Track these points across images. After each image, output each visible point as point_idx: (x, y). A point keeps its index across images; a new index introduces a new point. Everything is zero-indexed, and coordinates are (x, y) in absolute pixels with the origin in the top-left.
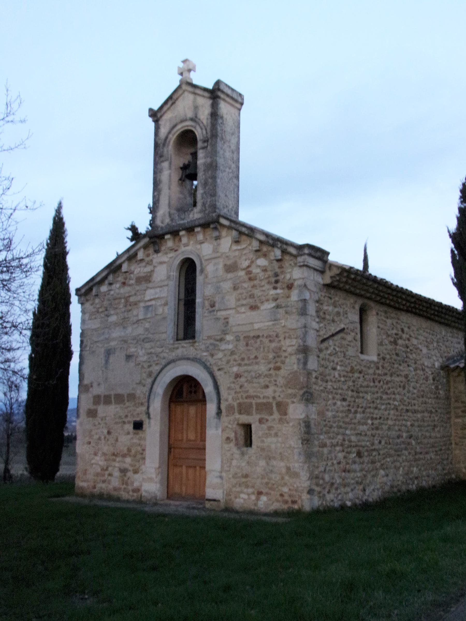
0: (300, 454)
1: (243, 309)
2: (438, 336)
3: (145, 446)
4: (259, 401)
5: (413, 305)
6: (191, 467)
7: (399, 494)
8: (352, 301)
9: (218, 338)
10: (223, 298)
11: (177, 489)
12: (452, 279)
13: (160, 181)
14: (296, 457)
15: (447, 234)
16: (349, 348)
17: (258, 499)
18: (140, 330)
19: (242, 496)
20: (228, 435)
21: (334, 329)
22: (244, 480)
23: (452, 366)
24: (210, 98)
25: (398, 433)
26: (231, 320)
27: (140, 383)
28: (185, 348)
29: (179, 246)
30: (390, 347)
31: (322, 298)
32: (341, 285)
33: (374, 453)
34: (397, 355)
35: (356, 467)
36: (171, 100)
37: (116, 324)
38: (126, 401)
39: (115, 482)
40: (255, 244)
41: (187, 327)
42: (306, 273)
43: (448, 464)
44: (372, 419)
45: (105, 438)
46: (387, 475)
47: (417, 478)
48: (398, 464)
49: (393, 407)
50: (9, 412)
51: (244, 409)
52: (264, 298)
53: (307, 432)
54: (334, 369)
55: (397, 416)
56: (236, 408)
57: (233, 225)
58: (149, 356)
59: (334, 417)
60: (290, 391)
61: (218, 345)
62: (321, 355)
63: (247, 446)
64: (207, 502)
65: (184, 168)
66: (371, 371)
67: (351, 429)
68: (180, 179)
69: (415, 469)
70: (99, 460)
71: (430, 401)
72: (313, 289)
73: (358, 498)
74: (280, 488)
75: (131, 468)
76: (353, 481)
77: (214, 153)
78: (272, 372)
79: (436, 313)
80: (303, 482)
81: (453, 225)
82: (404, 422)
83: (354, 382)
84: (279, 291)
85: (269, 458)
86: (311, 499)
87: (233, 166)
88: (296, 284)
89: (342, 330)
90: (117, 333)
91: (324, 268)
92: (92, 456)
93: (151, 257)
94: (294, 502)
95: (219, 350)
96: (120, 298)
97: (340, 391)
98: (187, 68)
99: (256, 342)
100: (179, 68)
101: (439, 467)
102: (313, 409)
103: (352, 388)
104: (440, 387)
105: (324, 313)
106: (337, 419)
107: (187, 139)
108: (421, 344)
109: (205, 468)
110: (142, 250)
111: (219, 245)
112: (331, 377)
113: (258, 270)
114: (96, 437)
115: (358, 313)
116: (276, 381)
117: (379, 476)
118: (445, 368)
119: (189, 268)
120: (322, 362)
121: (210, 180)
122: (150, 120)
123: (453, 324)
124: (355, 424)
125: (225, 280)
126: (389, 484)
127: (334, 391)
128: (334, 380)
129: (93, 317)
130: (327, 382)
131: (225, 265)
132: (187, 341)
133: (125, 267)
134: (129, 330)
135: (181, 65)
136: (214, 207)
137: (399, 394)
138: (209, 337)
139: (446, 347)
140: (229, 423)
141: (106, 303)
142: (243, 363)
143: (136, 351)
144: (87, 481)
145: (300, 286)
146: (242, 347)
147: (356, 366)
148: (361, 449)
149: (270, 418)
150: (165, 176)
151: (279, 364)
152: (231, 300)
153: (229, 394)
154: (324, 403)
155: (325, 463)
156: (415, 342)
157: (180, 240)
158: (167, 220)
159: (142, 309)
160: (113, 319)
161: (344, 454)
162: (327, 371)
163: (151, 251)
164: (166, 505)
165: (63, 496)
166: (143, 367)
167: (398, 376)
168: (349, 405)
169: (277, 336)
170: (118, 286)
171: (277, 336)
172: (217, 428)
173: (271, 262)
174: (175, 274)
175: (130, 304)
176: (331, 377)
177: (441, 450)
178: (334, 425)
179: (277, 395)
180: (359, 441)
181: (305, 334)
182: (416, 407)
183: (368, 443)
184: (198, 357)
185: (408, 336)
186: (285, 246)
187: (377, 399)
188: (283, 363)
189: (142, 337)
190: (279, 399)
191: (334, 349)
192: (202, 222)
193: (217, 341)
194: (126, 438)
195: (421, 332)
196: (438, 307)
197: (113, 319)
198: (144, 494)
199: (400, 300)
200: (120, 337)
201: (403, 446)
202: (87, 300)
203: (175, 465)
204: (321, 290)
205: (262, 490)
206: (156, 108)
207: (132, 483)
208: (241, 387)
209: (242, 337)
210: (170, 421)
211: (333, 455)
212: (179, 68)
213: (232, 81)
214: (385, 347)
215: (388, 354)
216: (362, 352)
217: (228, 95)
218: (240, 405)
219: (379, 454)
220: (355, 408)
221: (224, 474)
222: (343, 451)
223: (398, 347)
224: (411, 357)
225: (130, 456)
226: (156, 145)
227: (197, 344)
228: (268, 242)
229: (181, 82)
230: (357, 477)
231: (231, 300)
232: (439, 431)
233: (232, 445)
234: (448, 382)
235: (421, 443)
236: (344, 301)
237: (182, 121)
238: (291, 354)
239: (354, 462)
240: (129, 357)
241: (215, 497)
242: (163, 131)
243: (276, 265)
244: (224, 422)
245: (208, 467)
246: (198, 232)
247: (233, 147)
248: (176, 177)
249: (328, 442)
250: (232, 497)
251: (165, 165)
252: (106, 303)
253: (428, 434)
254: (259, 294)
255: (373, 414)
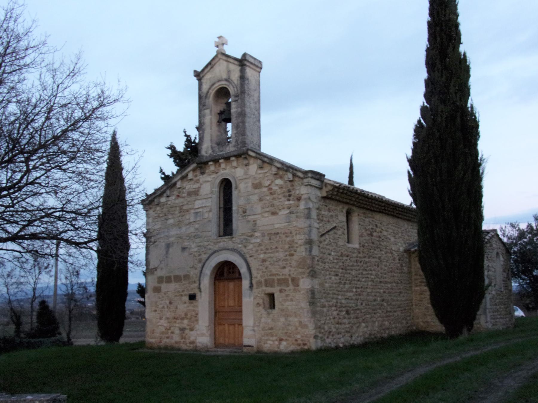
0: (308, 312)
1: (266, 215)
2: (403, 229)
3: (198, 311)
4: (279, 277)
5: (383, 208)
6: (231, 325)
7: (375, 340)
8: (341, 207)
9: (250, 234)
10: (252, 207)
11: (221, 341)
12: (409, 191)
13: (204, 124)
14: (305, 315)
15: (406, 160)
16: (340, 239)
17: (280, 344)
18: (192, 230)
19: (269, 342)
20: (258, 302)
21: (329, 227)
22: (270, 331)
23: (412, 250)
24: (240, 65)
25: (374, 298)
26: (258, 222)
27: (193, 267)
28: (225, 242)
29: (219, 170)
30: (367, 238)
31: (321, 206)
32: (334, 197)
33: (358, 312)
34: (373, 243)
35: (346, 321)
36: (210, 65)
37: (173, 225)
38: (182, 280)
39: (176, 338)
40: (274, 170)
41: (226, 227)
42: (310, 190)
43: (410, 320)
44: (356, 288)
45: (167, 307)
46: (367, 327)
47: (388, 329)
48: (374, 319)
49: (370, 279)
50: (70, 292)
51: (268, 283)
52: (281, 207)
53: (313, 298)
54: (330, 254)
55: (374, 286)
56: (263, 282)
57: (258, 156)
58: (199, 248)
59: (331, 287)
60: (300, 270)
61: (249, 240)
62: (321, 245)
63: (271, 309)
64: (244, 348)
65: (221, 113)
66: (355, 255)
67: (342, 295)
68: (218, 122)
69: (386, 323)
70: (164, 323)
71: (396, 275)
72: (315, 200)
73: (347, 342)
74: (295, 335)
75: (188, 327)
76: (343, 331)
77: (243, 105)
78: (288, 257)
79: (400, 213)
80: (311, 330)
81: (410, 154)
82: (378, 290)
83: (343, 263)
84: (291, 202)
85: (287, 316)
86: (316, 342)
87: (256, 113)
88: (303, 197)
89: (335, 228)
90: (174, 232)
91: (322, 186)
92: (158, 320)
93: (198, 178)
94: (305, 344)
95: (250, 243)
96: (176, 207)
97: (334, 269)
98: (221, 42)
99: (276, 237)
100: (215, 42)
101: (404, 322)
102: (316, 281)
103: (342, 267)
104: (404, 265)
105: (323, 217)
106: (332, 288)
107: (223, 93)
108: (390, 235)
109: (242, 325)
110: (191, 172)
111: (248, 169)
112: (328, 260)
113: (277, 188)
114: (161, 306)
115: (345, 215)
116: (290, 263)
117: (362, 327)
118: (407, 251)
119: (226, 186)
120: (322, 250)
121: (241, 124)
122: (195, 78)
123: (413, 219)
124: (344, 292)
125: (253, 194)
126: (368, 332)
127: (330, 270)
128: (329, 262)
129: (155, 220)
130: (325, 263)
131: (253, 184)
132: (227, 237)
133: (179, 185)
134: (184, 229)
135: (217, 40)
136: (244, 143)
137: (374, 270)
138: (243, 234)
139: (408, 236)
140: (259, 293)
141: (165, 210)
142: (267, 251)
143: (189, 245)
144: (155, 338)
145: (305, 199)
146: (266, 240)
147: (344, 251)
148: (349, 308)
149: (287, 289)
150: (207, 120)
151: (292, 252)
152: (258, 208)
153: (258, 273)
154: (323, 278)
155: (325, 318)
156: (385, 233)
157: (220, 166)
158: (210, 152)
159: (193, 215)
160: (171, 221)
161: (337, 312)
162: (325, 256)
163: (198, 173)
164: (215, 351)
165: (138, 349)
166: (195, 256)
167: (374, 258)
168: (340, 279)
169: (291, 233)
170: (174, 198)
171: (291, 233)
172: (250, 296)
173: (285, 182)
174: (216, 189)
175: (183, 211)
176: (328, 260)
177: (405, 309)
178: (331, 292)
179: (291, 273)
180: (347, 303)
181: (310, 231)
182: (387, 280)
183: (353, 305)
184: (235, 248)
185: (380, 230)
186: (295, 172)
187: (359, 274)
188: (295, 251)
189: (193, 235)
190: (293, 276)
191: (330, 241)
192: (236, 153)
193: (249, 236)
194: (183, 306)
195: (390, 226)
196: (402, 208)
197: (171, 221)
198: (198, 344)
199: (374, 205)
200: (177, 234)
201: (377, 307)
202: (150, 208)
203: (220, 324)
204: (320, 201)
205: (282, 337)
206: (199, 70)
207: (189, 337)
208: (266, 268)
209: (266, 234)
210: (215, 293)
211: (330, 312)
212: (215, 42)
213: (255, 53)
214: (364, 238)
215: (367, 242)
216: (348, 242)
217: (251, 63)
218: (266, 281)
219: (361, 312)
220: (344, 281)
221: (256, 328)
222: (337, 310)
223: (373, 238)
224: (382, 244)
225: (187, 319)
226: (200, 97)
227: (234, 239)
228: (283, 168)
229: (218, 52)
230: (346, 328)
231: (258, 208)
232: (404, 296)
233: (261, 308)
234: (410, 261)
235: (391, 304)
236: (336, 208)
237: (219, 81)
238: (301, 245)
239: (345, 318)
240: (184, 249)
241: (250, 344)
242: (205, 87)
243: (289, 184)
244: (255, 292)
245: (244, 324)
246: (233, 161)
247: (256, 100)
248: (215, 120)
249: (327, 304)
250: (262, 343)
251: (207, 111)
252: (165, 210)
253: (395, 298)
254: (278, 204)
255: (356, 284)
